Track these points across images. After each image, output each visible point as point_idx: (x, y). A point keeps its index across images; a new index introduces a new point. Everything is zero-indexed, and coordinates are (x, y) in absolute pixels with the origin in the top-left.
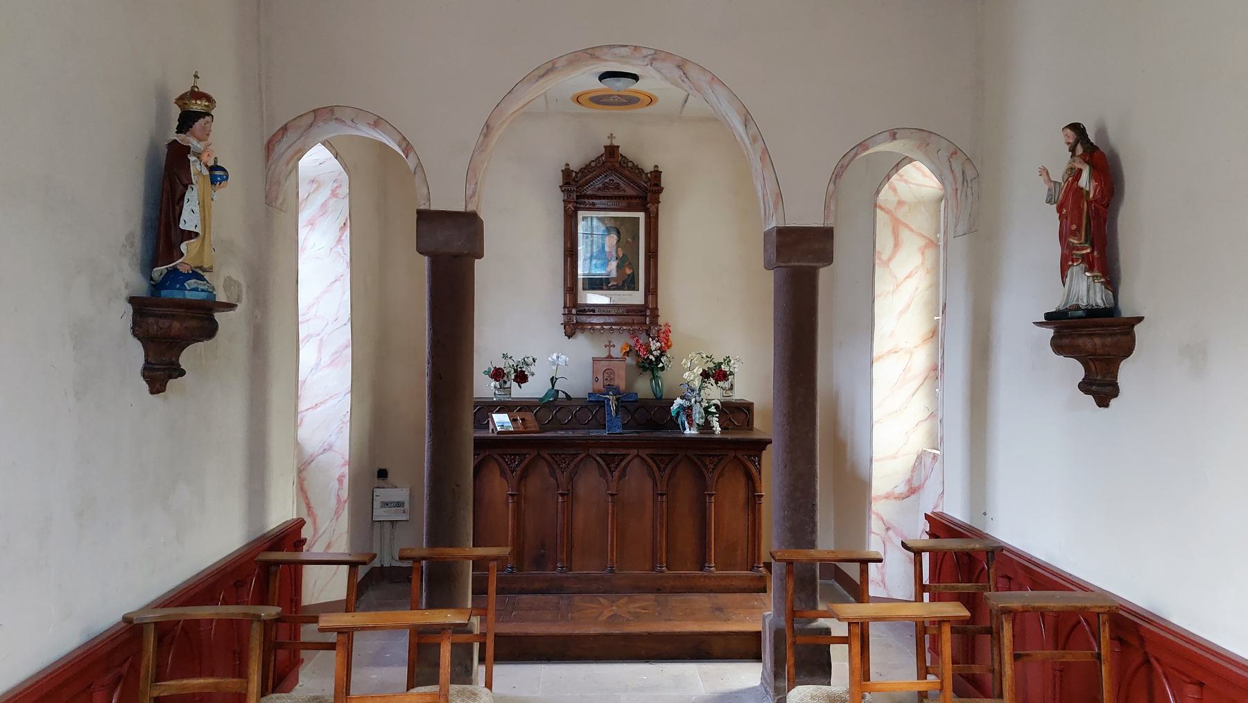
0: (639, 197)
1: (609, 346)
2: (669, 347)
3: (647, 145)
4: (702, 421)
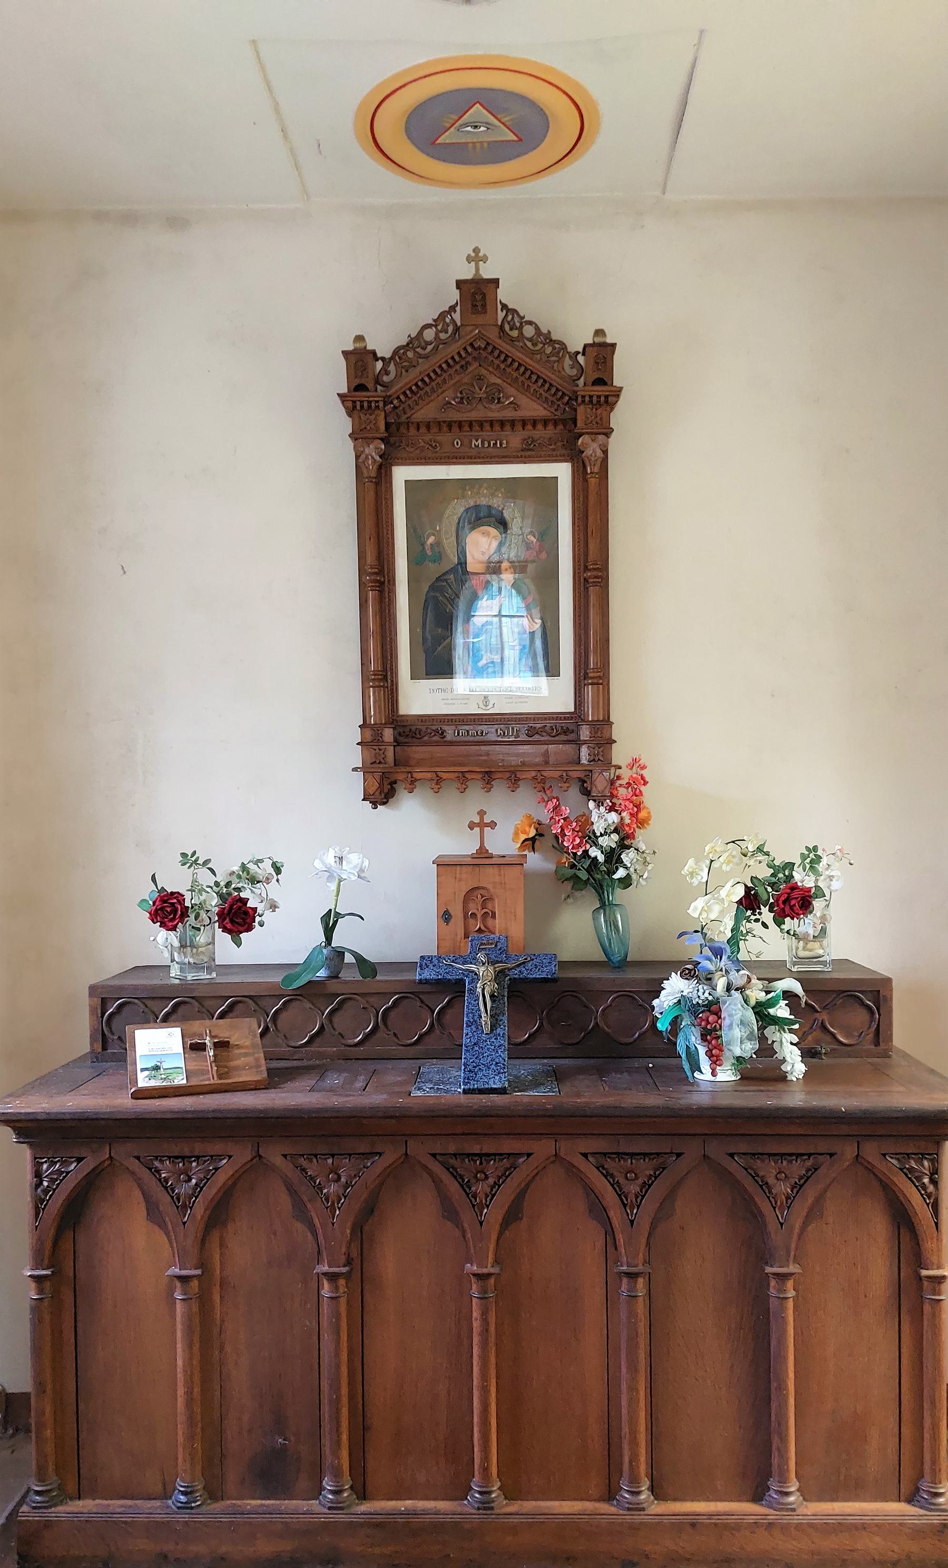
0: (564, 422)
1: (482, 825)
2: (642, 823)
3: (569, 267)
4: (748, 1049)
